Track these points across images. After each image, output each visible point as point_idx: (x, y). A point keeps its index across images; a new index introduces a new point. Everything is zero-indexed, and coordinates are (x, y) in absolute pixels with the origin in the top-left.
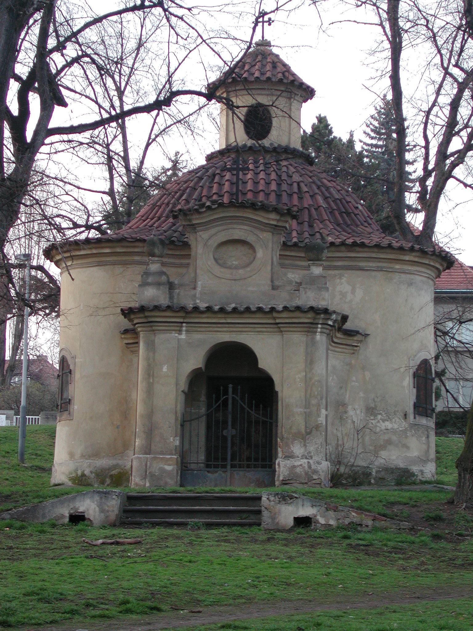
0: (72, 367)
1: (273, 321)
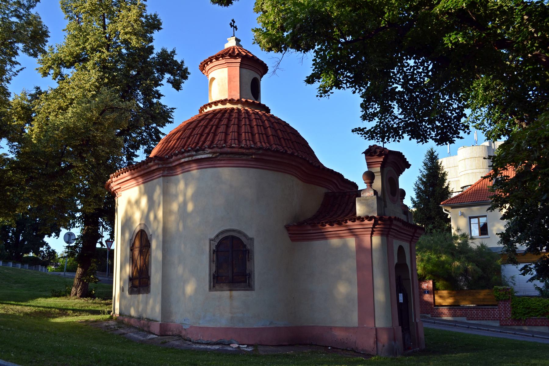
0: (248, 247)
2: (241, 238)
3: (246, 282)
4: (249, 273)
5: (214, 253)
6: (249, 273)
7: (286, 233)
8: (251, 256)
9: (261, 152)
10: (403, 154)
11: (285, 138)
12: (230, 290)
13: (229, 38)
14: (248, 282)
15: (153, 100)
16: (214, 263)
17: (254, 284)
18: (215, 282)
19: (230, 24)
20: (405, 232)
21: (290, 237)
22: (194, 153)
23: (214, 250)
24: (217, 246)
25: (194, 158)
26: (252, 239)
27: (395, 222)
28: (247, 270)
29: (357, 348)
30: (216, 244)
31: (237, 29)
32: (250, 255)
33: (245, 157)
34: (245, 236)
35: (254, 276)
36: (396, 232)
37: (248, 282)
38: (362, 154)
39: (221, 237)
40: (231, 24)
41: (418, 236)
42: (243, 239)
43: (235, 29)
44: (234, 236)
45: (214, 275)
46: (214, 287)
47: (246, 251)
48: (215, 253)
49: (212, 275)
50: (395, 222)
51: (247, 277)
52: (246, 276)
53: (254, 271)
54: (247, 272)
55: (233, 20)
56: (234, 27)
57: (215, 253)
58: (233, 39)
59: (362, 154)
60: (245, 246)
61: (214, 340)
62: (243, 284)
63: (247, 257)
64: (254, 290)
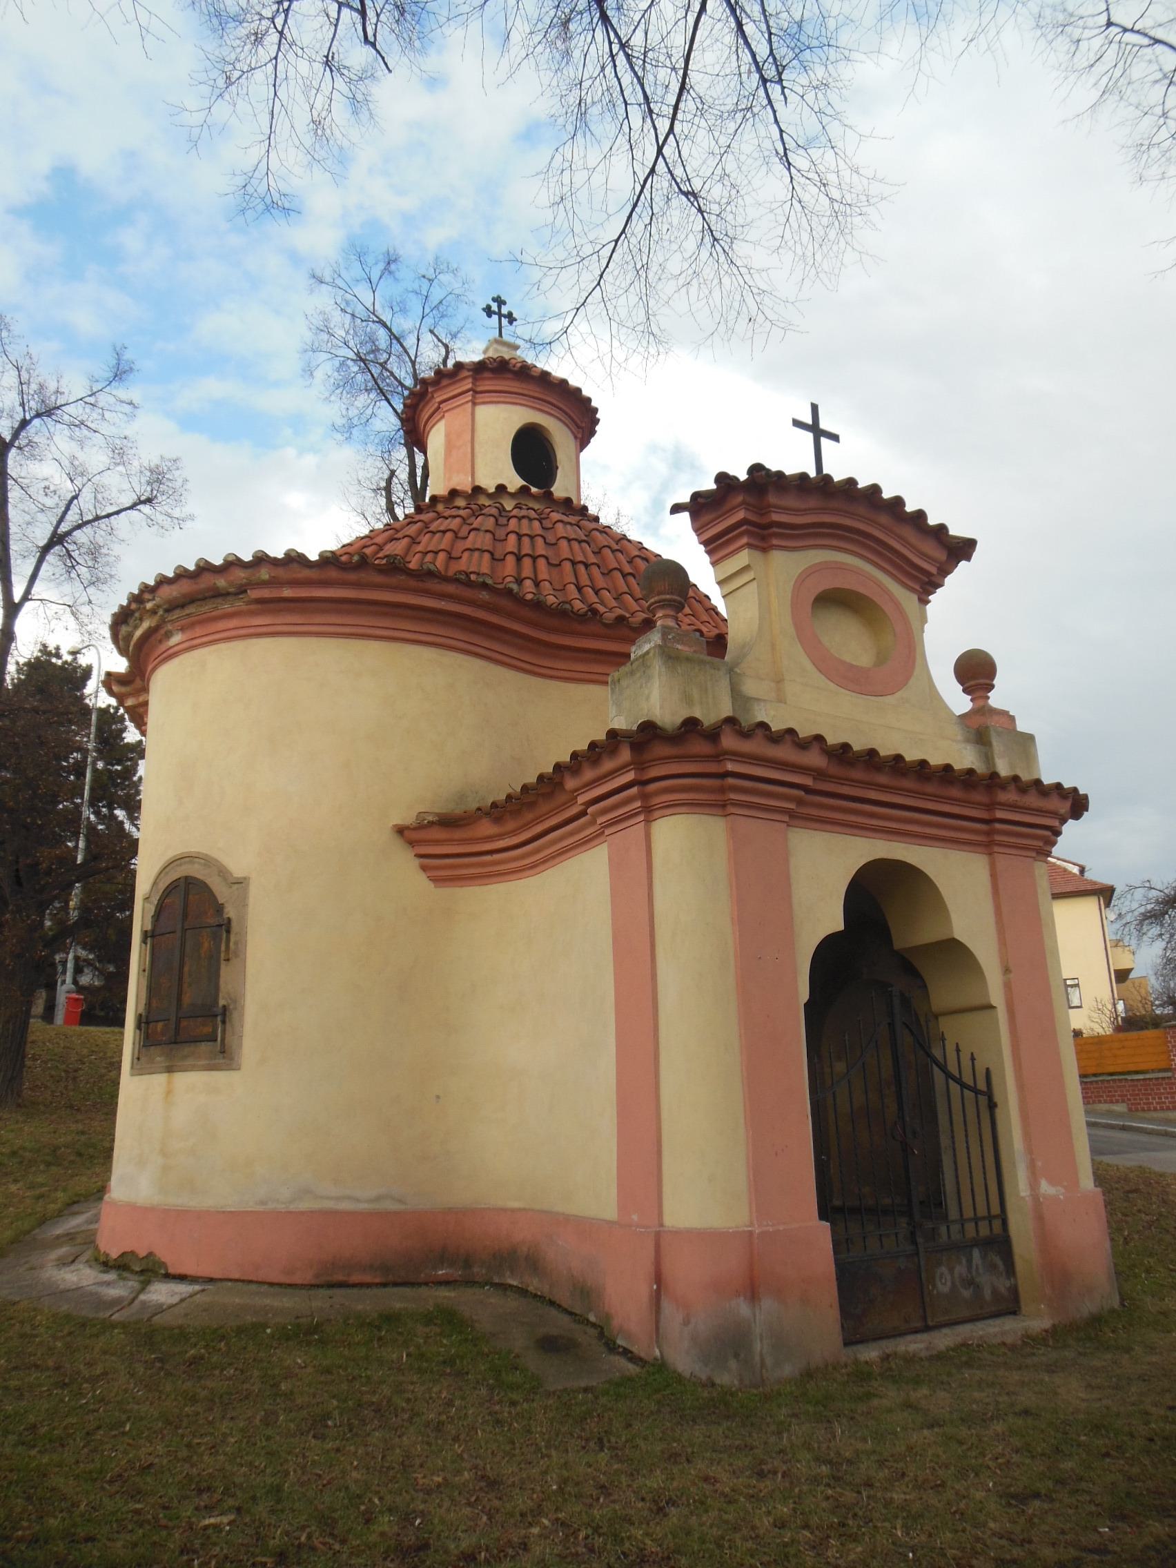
0: (230, 912)
1: (984, 815)
2: (208, 881)
3: (216, 1040)
7: (405, 865)
8: (236, 943)
11: (580, 558)
12: (170, 1070)
17: (240, 1046)
21: (424, 868)
26: (241, 883)
32: (233, 938)
33: (227, 607)
34: (223, 872)
35: (242, 1015)
37: (219, 1039)
39: (162, 886)
43: (505, 321)
46: (138, 1059)
48: (149, 940)
50: (729, 741)
51: (219, 1019)
52: (216, 1016)
54: (222, 1002)
56: (500, 315)
57: (149, 940)
59: (676, 509)
60: (220, 909)
62: (204, 1047)
63: (223, 948)
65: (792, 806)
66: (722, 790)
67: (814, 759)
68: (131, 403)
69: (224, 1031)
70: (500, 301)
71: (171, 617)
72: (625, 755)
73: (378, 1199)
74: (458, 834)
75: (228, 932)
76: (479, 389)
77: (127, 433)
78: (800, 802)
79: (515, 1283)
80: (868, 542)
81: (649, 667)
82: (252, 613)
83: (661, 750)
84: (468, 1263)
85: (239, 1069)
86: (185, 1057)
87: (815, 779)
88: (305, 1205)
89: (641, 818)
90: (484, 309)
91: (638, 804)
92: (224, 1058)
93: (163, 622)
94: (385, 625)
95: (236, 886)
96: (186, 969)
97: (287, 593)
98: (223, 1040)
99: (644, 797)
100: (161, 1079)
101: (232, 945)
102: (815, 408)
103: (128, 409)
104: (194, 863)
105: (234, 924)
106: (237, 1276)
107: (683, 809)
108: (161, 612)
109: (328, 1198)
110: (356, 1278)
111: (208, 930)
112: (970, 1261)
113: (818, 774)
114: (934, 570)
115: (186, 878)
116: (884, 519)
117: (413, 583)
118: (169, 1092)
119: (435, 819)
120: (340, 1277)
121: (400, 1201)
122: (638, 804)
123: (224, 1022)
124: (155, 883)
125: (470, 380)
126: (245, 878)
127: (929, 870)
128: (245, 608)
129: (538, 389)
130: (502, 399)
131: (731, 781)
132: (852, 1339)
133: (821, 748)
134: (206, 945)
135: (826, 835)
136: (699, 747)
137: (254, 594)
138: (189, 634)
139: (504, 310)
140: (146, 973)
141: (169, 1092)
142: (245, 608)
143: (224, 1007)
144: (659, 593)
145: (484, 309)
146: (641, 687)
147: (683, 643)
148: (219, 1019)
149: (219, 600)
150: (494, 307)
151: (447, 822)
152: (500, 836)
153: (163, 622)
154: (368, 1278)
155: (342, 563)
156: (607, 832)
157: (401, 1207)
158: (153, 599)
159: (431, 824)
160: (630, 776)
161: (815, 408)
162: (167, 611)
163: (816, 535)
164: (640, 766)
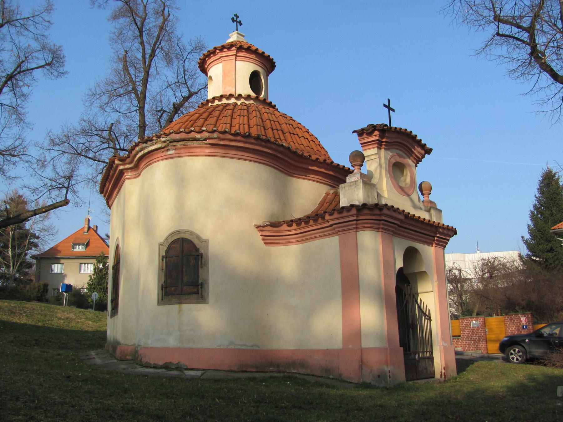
0: (202, 251)
3: (198, 294)
4: (202, 283)
5: (163, 260)
6: (202, 283)
8: (204, 261)
9: (215, 135)
10: (275, 64)
12: (180, 303)
13: (231, 34)
14: (200, 293)
15: (529, 253)
16: (162, 272)
17: (208, 295)
18: (164, 294)
19: (242, 24)
20: (413, 228)
22: (144, 145)
23: (163, 257)
24: (167, 251)
25: (146, 151)
27: (385, 211)
28: (200, 279)
29: (340, 375)
30: (166, 249)
31: (241, 24)
34: (198, 237)
35: (208, 286)
36: (396, 226)
37: (200, 293)
38: (354, 132)
39: (170, 241)
40: (233, 19)
41: (448, 238)
42: (196, 242)
43: (238, 24)
44: (185, 238)
45: (162, 285)
46: (162, 300)
47: (198, 255)
48: (164, 259)
49: (160, 286)
51: (200, 287)
52: (198, 286)
53: (208, 279)
54: (200, 281)
55: (236, 15)
56: (237, 22)
57: (164, 259)
58: (234, 34)
59: (354, 132)
61: (161, 363)
62: (194, 296)
63: (200, 263)
64: (208, 303)
65: (394, 230)
66: (379, 224)
67: (402, 217)
68: (49, 22)
69: (202, 291)
70: (236, 16)
71: (171, 144)
72: (354, 211)
73: (252, 346)
74: (275, 229)
75: (202, 257)
76: (238, 55)
77: (45, 34)
78: (396, 228)
79: (295, 371)
80: (405, 147)
81: (358, 185)
82: (207, 147)
83: (366, 211)
84: (278, 366)
85: (158, 305)
86: (186, 299)
87: (401, 223)
88: (232, 347)
89: (355, 230)
90: (231, 19)
91: (355, 226)
92: (202, 300)
93: (168, 145)
94: (249, 156)
95: (204, 242)
96: (184, 270)
97: (222, 142)
98: (201, 294)
99: (357, 224)
100: (176, 306)
101: (203, 262)
102: (389, 100)
103: (47, 24)
104: (186, 233)
105: (204, 255)
106: (213, 368)
107: (369, 229)
108: (168, 142)
109: (239, 345)
110: (248, 370)
111: (193, 257)
112: (425, 363)
113: (401, 221)
114: (420, 157)
115: (183, 238)
116: (410, 141)
117: (263, 143)
118: (180, 311)
119: (269, 224)
120: (244, 369)
121: (258, 347)
122: (355, 226)
123: (201, 288)
124: (167, 239)
125: (235, 51)
126: (207, 240)
127: (417, 247)
128: (204, 145)
129: (247, 54)
130: (246, 60)
131: (382, 222)
132: (407, 380)
133: (387, 208)
134: (192, 262)
135: (399, 239)
136: (377, 212)
137: (208, 141)
138: (176, 152)
139: (238, 20)
140: (164, 270)
141: (180, 311)
142: (204, 145)
143: (202, 283)
144: (357, 162)
145: (231, 19)
146: (355, 190)
147: (365, 178)
148: (200, 287)
149: (195, 142)
150: (235, 19)
151: (274, 225)
152: (289, 230)
153: (168, 145)
154: (252, 370)
155: (300, 155)
156: (339, 233)
157: (259, 349)
158: (166, 138)
159: (267, 225)
160: (355, 218)
161: (389, 100)
162: (170, 142)
163: (399, 146)
164: (357, 215)
